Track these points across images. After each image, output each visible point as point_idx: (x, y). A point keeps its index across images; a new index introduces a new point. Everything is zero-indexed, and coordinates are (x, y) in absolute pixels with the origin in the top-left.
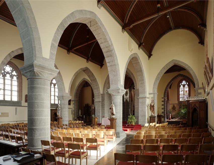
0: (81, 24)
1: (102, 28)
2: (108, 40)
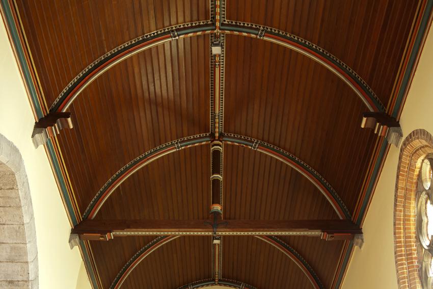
0: (72, 76)
1: (24, 209)
2: (30, 258)
